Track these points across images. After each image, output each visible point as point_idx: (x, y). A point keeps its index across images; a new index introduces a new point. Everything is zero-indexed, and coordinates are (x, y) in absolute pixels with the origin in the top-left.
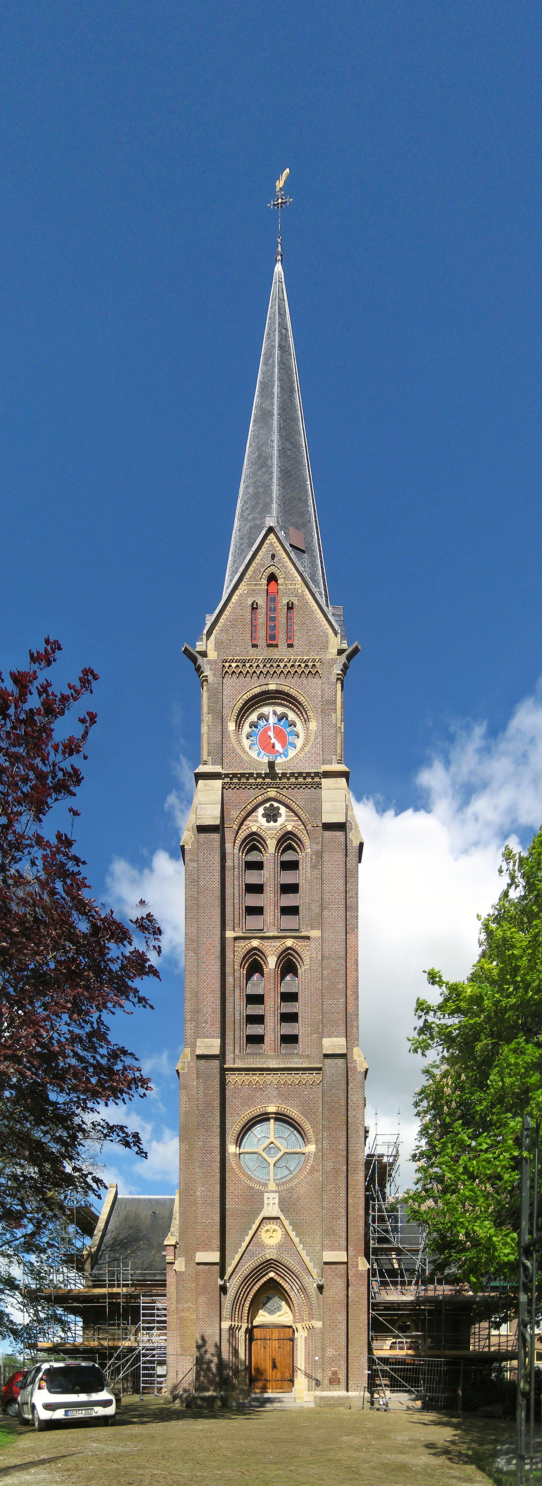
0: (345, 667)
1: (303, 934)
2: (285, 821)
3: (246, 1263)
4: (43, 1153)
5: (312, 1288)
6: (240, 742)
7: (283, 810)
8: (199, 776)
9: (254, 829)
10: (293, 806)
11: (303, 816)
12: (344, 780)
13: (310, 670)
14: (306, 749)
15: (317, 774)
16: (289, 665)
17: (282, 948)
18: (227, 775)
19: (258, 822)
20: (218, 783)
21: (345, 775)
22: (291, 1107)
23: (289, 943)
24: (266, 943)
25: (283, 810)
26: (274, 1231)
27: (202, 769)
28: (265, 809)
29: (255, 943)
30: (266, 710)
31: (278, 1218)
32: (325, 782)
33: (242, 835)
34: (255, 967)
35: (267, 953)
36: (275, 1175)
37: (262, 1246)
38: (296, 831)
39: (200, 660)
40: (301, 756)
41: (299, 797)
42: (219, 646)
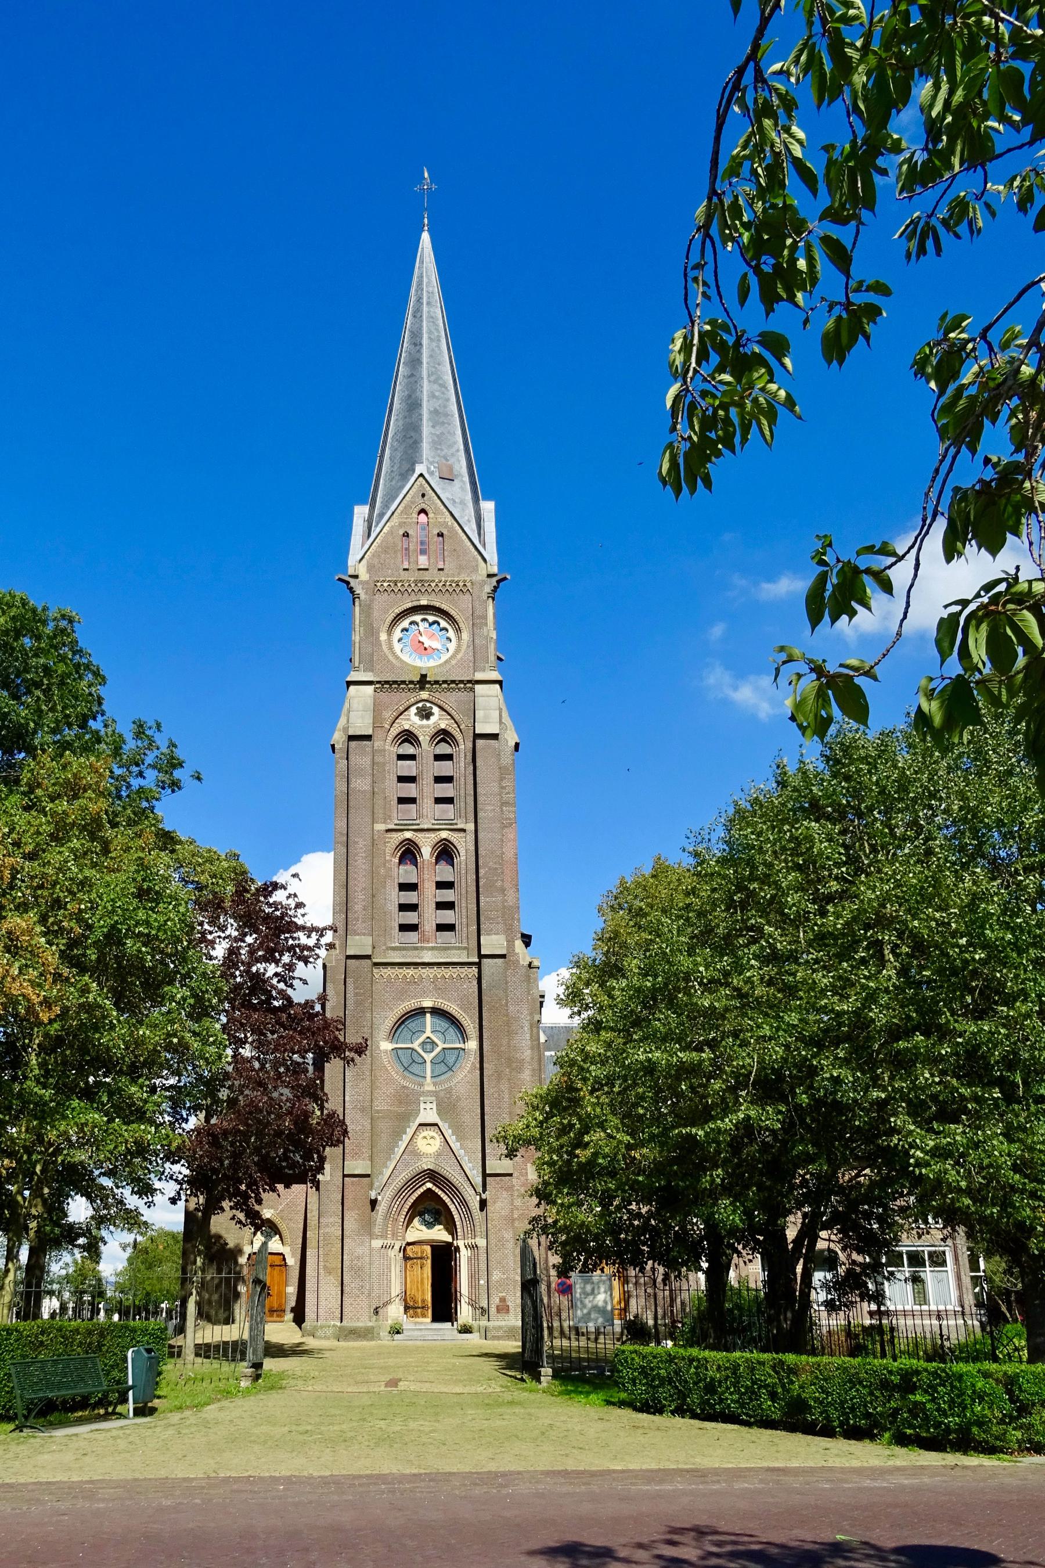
0: (495, 589)
1: (459, 826)
2: (438, 720)
3: (400, 1174)
4: (262, 1220)
5: (474, 1202)
6: (391, 648)
7: (435, 710)
8: (349, 684)
9: (407, 727)
10: (446, 707)
11: (456, 717)
12: (497, 686)
13: (462, 589)
14: (459, 657)
15: (469, 682)
16: (440, 585)
17: (437, 840)
18: (379, 682)
19: (412, 721)
20: (370, 689)
21: (500, 683)
22: (449, 1001)
23: (444, 834)
24: (420, 835)
25: (435, 710)
26: (432, 1138)
27: (353, 676)
28: (418, 708)
29: (408, 835)
30: (417, 618)
31: (436, 1125)
32: (477, 687)
33: (394, 731)
34: (409, 853)
35: (420, 844)
36: (432, 1071)
37: (417, 1154)
38: (449, 729)
39: (353, 583)
40: (453, 662)
41: (452, 699)
42: (370, 568)
